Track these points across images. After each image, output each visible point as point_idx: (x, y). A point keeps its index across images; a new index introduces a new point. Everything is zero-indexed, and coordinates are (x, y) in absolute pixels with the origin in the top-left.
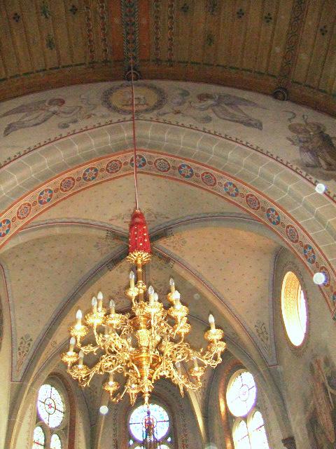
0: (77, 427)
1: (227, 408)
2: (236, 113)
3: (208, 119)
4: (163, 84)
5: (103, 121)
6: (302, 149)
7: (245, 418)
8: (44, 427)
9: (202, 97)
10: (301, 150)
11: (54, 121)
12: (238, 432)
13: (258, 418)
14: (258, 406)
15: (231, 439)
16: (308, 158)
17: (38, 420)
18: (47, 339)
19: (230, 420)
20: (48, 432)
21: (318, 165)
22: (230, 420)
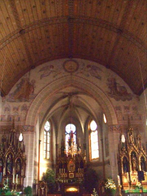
0: (53, 134)
1: (90, 128)
2: (95, 73)
3: (88, 76)
4: (79, 60)
5: (64, 75)
6: (109, 87)
7: (94, 131)
8: (46, 131)
9: (88, 66)
10: (108, 88)
11: (52, 75)
12: (92, 134)
13: (96, 132)
14: (97, 129)
15: (90, 135)
16: (109, 91)
17: (45, 130)
18: (105, 187)
19: (90, 131)
20: (47, 132)
21: (110, 93)
22: (90, 131)
